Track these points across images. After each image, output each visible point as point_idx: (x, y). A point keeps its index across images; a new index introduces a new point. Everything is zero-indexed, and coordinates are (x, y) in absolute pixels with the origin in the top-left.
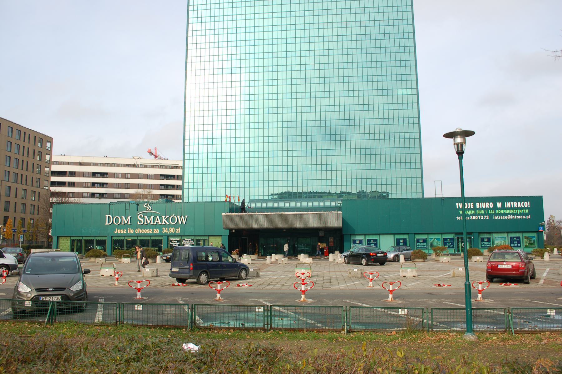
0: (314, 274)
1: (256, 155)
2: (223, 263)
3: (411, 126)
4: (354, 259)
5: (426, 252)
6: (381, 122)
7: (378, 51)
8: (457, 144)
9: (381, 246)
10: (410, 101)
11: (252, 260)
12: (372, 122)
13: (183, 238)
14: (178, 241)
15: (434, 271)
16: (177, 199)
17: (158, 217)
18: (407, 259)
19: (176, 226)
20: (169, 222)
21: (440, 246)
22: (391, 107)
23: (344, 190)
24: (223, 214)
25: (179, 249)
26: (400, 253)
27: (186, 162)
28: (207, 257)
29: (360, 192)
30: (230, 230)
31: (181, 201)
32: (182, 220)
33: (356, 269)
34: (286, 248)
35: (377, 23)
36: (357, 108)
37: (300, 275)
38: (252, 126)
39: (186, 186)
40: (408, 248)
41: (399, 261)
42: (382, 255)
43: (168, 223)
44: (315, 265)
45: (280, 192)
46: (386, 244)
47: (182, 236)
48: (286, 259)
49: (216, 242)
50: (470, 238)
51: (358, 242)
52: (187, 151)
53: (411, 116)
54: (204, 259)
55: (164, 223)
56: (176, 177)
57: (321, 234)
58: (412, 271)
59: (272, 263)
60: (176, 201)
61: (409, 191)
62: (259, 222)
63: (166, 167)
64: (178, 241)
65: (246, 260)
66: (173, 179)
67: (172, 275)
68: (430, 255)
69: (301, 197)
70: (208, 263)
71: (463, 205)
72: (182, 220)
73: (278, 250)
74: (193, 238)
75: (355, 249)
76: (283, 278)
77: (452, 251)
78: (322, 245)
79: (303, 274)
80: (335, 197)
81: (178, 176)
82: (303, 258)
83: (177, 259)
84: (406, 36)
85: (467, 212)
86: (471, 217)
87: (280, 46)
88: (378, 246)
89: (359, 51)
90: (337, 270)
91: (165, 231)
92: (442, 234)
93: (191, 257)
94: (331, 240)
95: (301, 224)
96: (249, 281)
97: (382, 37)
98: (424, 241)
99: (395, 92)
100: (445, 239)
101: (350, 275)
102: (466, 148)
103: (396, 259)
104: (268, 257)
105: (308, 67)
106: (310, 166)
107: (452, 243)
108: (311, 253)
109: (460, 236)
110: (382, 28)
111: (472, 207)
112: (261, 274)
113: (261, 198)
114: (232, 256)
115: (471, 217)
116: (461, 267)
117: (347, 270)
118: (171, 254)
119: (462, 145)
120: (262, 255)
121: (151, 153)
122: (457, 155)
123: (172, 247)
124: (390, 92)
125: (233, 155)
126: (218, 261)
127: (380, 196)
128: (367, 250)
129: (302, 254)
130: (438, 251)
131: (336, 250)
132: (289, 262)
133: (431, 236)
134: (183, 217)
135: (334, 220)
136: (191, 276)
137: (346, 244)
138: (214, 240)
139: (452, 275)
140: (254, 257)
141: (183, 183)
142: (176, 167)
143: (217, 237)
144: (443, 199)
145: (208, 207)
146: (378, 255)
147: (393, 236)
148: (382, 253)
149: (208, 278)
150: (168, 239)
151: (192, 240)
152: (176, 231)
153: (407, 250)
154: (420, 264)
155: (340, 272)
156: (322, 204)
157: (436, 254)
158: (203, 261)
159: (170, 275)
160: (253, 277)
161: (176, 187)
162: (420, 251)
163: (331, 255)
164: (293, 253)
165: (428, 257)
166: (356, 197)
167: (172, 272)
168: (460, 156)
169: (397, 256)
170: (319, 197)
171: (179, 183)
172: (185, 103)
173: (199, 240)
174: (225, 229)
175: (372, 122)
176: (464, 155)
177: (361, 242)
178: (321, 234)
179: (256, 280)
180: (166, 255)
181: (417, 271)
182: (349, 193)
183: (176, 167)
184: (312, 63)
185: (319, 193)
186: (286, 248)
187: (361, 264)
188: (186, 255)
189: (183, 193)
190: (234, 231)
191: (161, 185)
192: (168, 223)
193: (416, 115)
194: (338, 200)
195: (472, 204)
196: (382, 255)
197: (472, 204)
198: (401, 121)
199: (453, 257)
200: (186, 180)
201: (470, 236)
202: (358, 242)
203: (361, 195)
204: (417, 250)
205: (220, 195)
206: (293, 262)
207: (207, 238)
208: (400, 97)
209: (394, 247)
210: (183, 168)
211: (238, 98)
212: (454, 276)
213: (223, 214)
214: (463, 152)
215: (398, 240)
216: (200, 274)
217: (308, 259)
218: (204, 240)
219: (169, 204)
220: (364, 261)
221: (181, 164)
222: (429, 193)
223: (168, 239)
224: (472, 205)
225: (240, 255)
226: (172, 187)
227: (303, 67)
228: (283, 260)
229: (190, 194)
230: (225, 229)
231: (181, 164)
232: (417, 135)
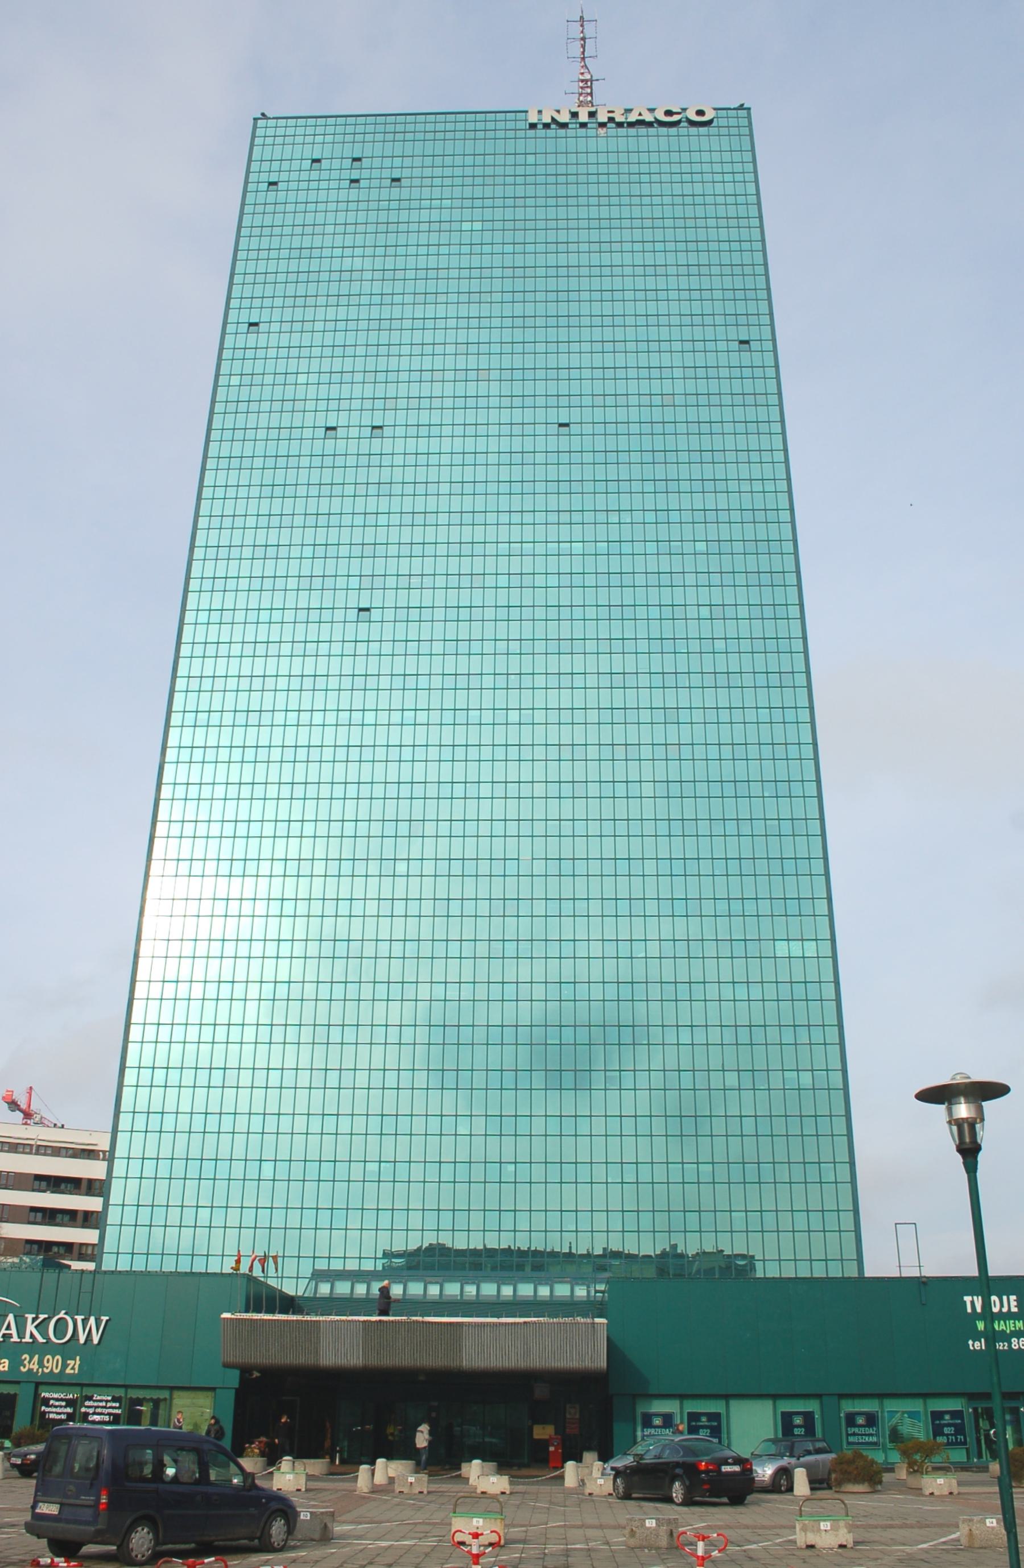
0: (516, 1532)
1: (345, 1125)
2: (209, 1489)
3: (819, 1050)
4: (645, 1483)
5: (879, 1457)
6: (729, 1036)
7: (718, 828)
8: (959, 1123)
9: (733, 1436)
10: (812, 976)
11: (310, 1478)
12: (700, 1037)
13: (87, 1391)
14: (70, 1403)
15: (904, 1526)
16: (82, 1257)
17: (11, 1318)
18: (817, 1483)
19: (68, 1350)
20: (45, 1334)
21: (922, 1436)
22: (756, 992)
23: (615, 1246)
24: (226, 1315)
25: (68, 1436)
26: (793, 1461)
27: (122, 1138)
28: (159, 1466)
29: (664, 1254)
30: (245, 1370)
31: (91, 1266)
32: (89, 1329)
33: (651, 1519)
34: (422, 1438)
35: (713, 752)
36: (655, 991)
37: (468, 1539)
38: (335, 1035)
39: (113, 1216)
40: (820, 1445)
41: (790, 1489)
42: (737, 1468)
43: (41, 1340)
44: (515, 1501)
45: (413, 1246)
46: (751, 1429)
47: (84, 1386)
48: (424, 1477)
49: (193, 1413)
50: (1015, 1411)
51: (657, 1421)
52: (126, 1104)
53: (815, 1020)
54: (148, 1470)
55: (27, 1339)
56: (84, 1185)
57: (541, 1391)
58: (835, 1528)
59: (376, 1490)
60: (76, 1265)
61: (818, 1254)
62: (341, 1349)
63: (57, 1151)
64: (70, 1403)
65: (288, 1477)
66: (77, 1191)
67: (37, 1526)
68: (891, 1470)
69: (477, 1267)
70: (161, 1486)
71: (987, 1304)
72: (89, 1329)
73: (400, 1449)
74: (120, 1392)
75: (651, 1445)
76: (409, 1549)
77: (958, 1455)
78: (542, 1432)
79: (476, 1536)
80: (587, 1269)
81: (90, 1181)
82: (482, 1477)
83: (58, 1469)
84: (797, 789)
85: (999, 1326)
86: (1014, 1340)
87: (425, 964)
88: (724, 1436)
89: (663, 828)
90: (590, 1520)
91: (30, 1364)
92: (925, 1396)
93: (106, 1465)
94: (573, 1413)
95: (474, 1357)
96: (292, 1555)
97: (729, 790)
98: (871, 1420)
99: (767, 948)
100: (937, 1415)
101: (632, 1542)
102: (986, 1135)
103: (782, 1483)
104: (364, 1468)
105: (511, 867)
106: (512, 1167)
107: (960, 1430)
108: (505, 1461)
109: (981, 1405)
110: (727, 765)
111: (1014, 1309)
112: (338, 1529)
113: (352, 1265)
114: (242, 1461)
115: (1014, 1340)
116: (989, 1511)
117: (623, 1522)
118: (40, 1447)
119: (972, 1126)
120: (343, 1462)
121: (13, 1105)
122: (959, 1158)
123: (45, 1423)
124: (753, 948)
125: (271, 1125)
126: (197, 1482)
127: (728, 1268)
128: (689, 1451)
129: (476, 1462)
130: (918, 1456)
131: (589, 1449)
132: (434, 1487)
133: (891, 1405)
134: (92, 1320)
135: (582, 1348)
136: (99, 1532)
137: (619, 1429)
138: (188, 1401)
139: (964, 1541)
140: (317, 1466)
141: (106, 1205)
142: (89, 1154)
143: (200, 1394)
144: (922, 1283)
145: (180, 1292)
146: (725, 1469)
147: (768, 1404)
148: (738, 1461)
149: (157, 1542)
150: (36, 1394)
151: (114, 1399)
152: (65, 1366)
153: (819, 1451)
154: (858, 1498)
155: (601, 1527)
156: (544, 1291)
157: (911, 1465)
158: (144, 1479)
159: (30, 1528)
160: (308, 1541)
161: (84, 1185)
162: (858, 1455)
163: (570, 1465)
164: (444, 1460)
165: (886, 1477)
166: (651, 1272)
167: (36, 1516)
168: (970, 1160)
169: (784, 1474)
170: (537, 1268)
171: (92, 1203)
172: (136, 956)
173: (140, 1402)
174: (227, 1365)
175: (700, 1037)
176: (981, 1157)
177: (668, 1420)
178: (541, 1391)
179: (318, 1553)
180: (25, 1449)
181: (851, 1528)
182: (630, 1256)
183: (89, 1154)
184: (525, 855)
185: (536, 1253)
186: (422, 1438)
187: (669, 1500)
188: (89, 1459)
189: (102, 1238)
190: (256, 1374)
191: (34, 1209)
192: (41, 1340)
193: (831, 1019)
194: (596, 1281)
195: (1013, 1298)
196: (737, 1468)
197: (1013, 1298)
198: (788, 1037)
199: (966, 1476)
200: (115, 1197)
201: (1013, 1404)
202: (657, 1421)
203: (670, 1265)
204: (849, 1453)
205: (217, 1247)
206: (444, 1487)
207: (164, 1394)
208: (782, 964)
209: (774, 1441)
210: (110, 1157)
211: (292, 1034)
212: (970, 1547)
213: (226, 1315)
214: (977, 1148)
215: (787, 1418)
216: (131, 1529)
217: (494, 1479)
218: (156, 1403)
219: (51, 1275)
220: (677, 1491)
221: (104, 1145)
222: (880, 1264)
223: (36, 1394)
224: (1013, 1303)
225: (272, 1458)
226: (67, 1218)
227: (498, 868)
228: (411, 1479)
229: (129, 1243)
230: (227, 1365)
231: (104, 1145)
232: (836, 1079)
